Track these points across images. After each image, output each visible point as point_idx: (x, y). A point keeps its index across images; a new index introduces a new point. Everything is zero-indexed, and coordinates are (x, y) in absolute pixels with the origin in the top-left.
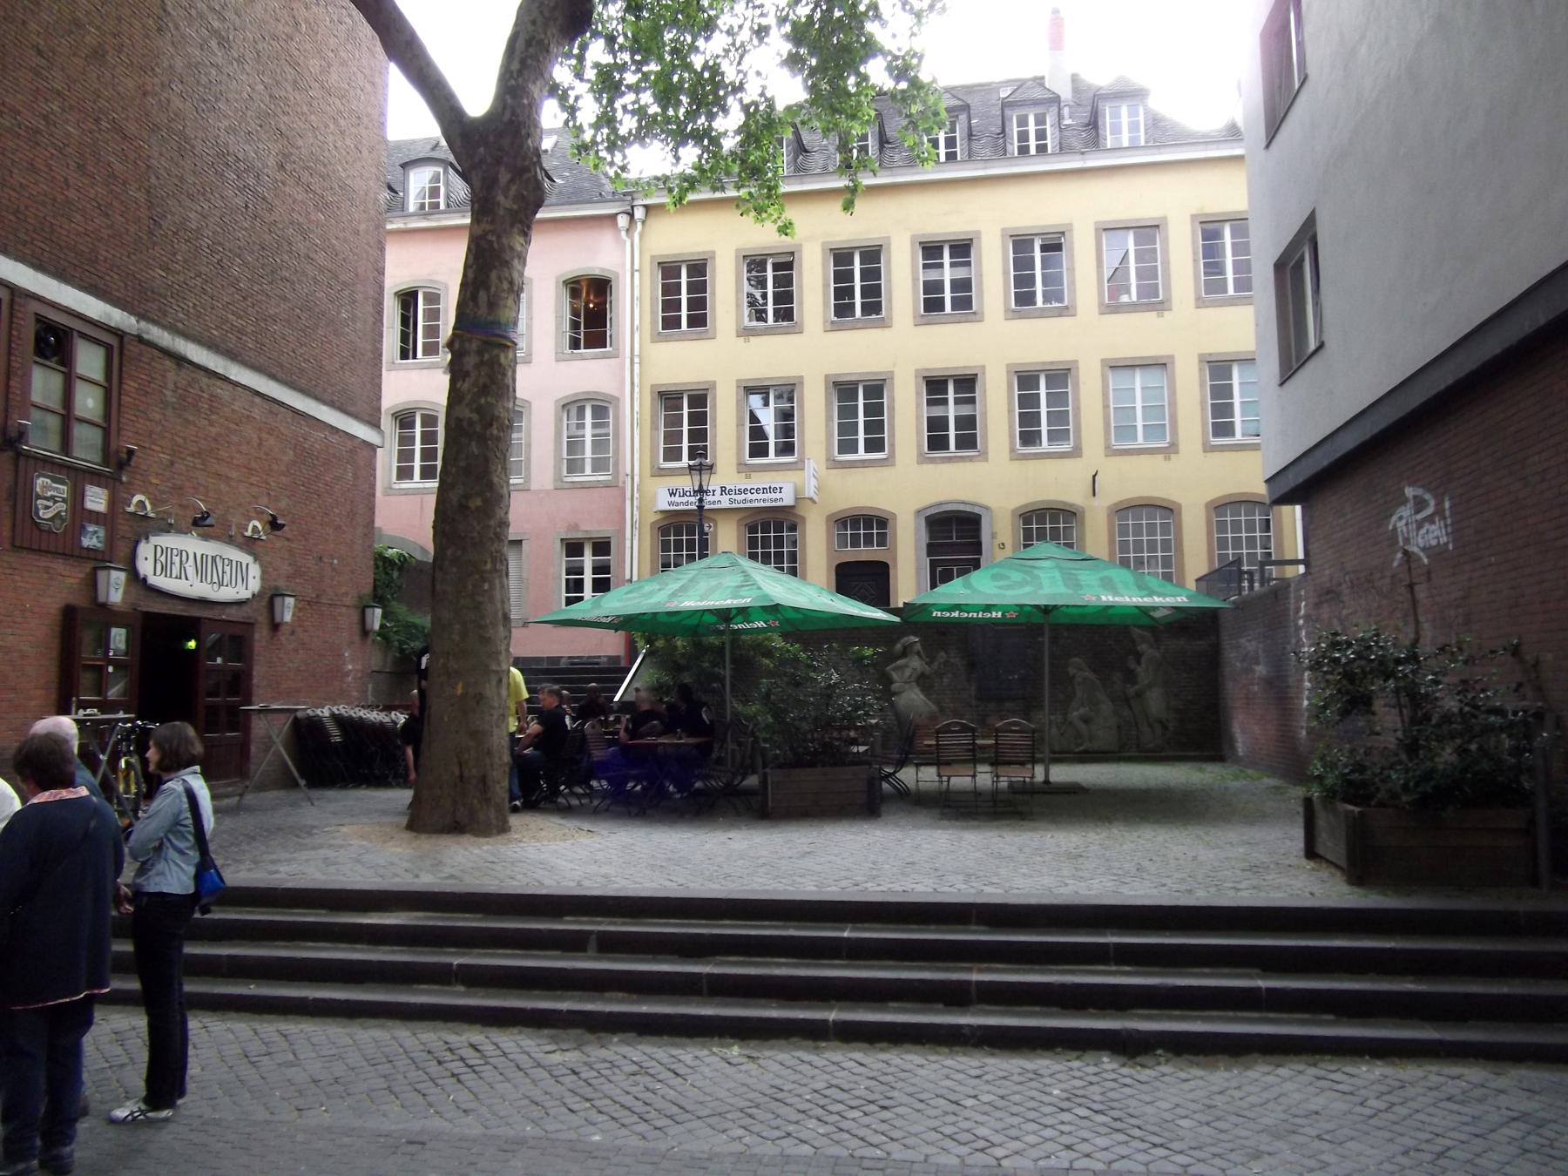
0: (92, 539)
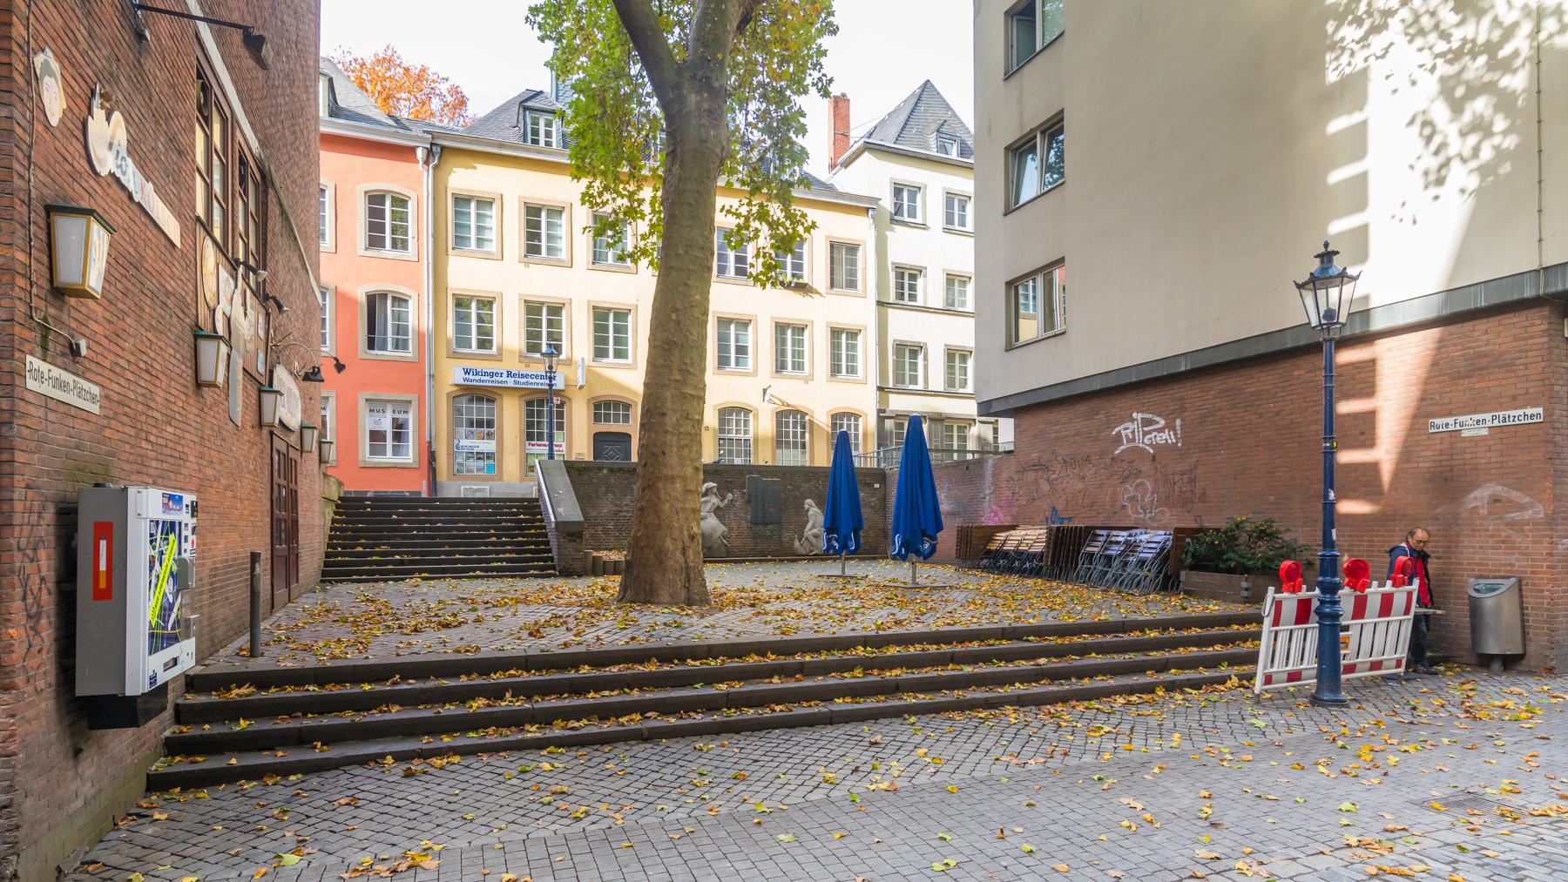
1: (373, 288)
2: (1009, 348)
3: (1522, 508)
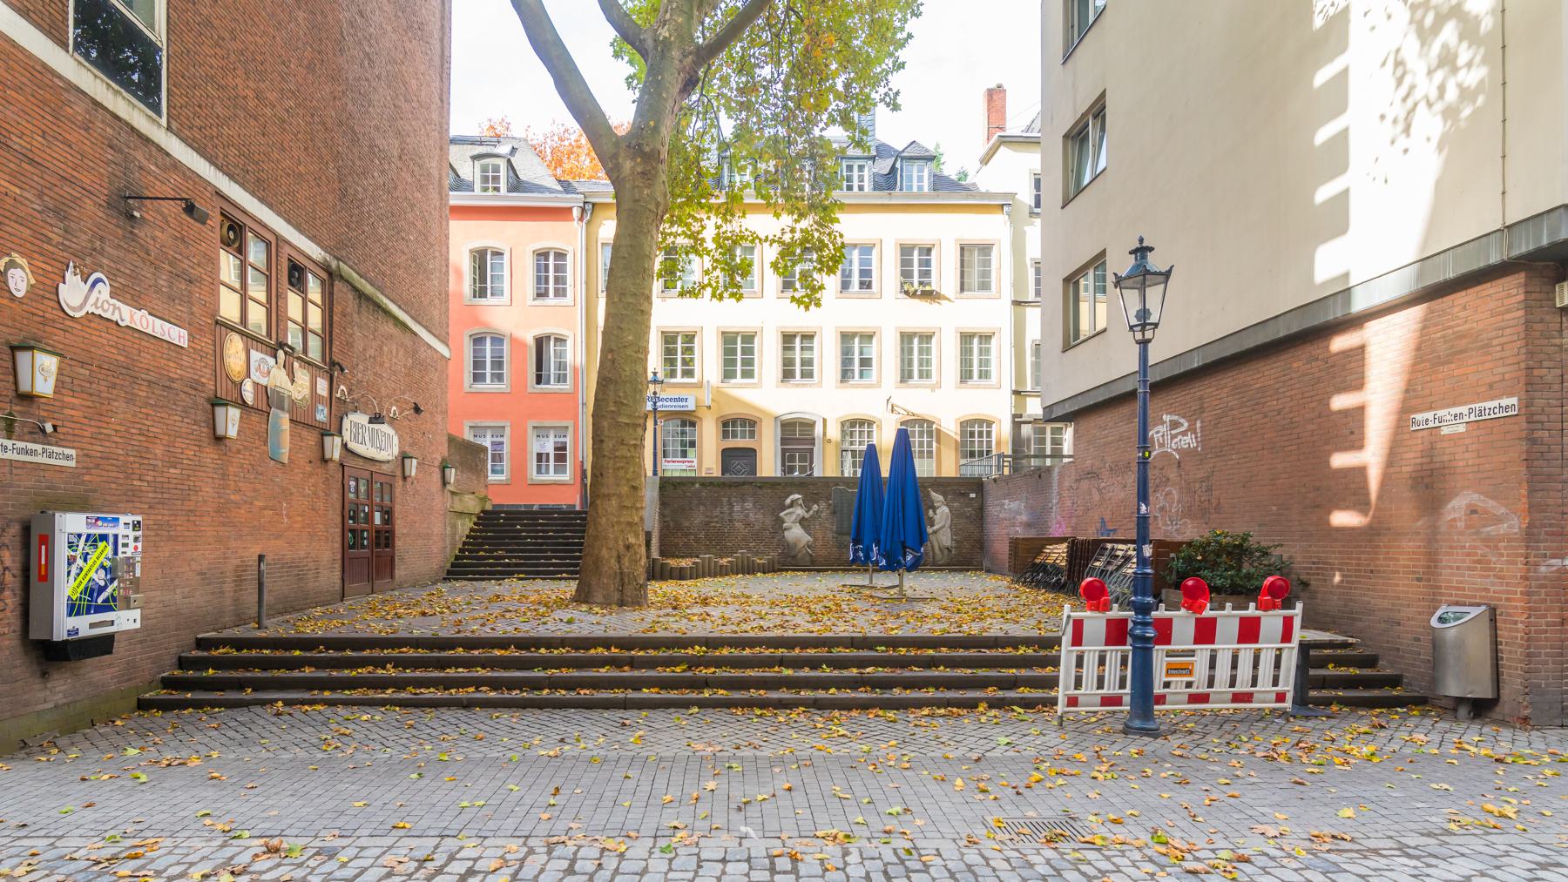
0: (322, 415)
1: (539, 332)
2: (1067, 347)
3: (1498, 520)
